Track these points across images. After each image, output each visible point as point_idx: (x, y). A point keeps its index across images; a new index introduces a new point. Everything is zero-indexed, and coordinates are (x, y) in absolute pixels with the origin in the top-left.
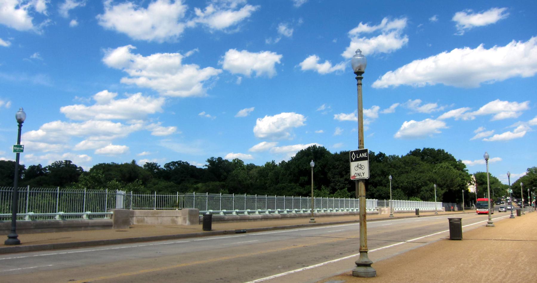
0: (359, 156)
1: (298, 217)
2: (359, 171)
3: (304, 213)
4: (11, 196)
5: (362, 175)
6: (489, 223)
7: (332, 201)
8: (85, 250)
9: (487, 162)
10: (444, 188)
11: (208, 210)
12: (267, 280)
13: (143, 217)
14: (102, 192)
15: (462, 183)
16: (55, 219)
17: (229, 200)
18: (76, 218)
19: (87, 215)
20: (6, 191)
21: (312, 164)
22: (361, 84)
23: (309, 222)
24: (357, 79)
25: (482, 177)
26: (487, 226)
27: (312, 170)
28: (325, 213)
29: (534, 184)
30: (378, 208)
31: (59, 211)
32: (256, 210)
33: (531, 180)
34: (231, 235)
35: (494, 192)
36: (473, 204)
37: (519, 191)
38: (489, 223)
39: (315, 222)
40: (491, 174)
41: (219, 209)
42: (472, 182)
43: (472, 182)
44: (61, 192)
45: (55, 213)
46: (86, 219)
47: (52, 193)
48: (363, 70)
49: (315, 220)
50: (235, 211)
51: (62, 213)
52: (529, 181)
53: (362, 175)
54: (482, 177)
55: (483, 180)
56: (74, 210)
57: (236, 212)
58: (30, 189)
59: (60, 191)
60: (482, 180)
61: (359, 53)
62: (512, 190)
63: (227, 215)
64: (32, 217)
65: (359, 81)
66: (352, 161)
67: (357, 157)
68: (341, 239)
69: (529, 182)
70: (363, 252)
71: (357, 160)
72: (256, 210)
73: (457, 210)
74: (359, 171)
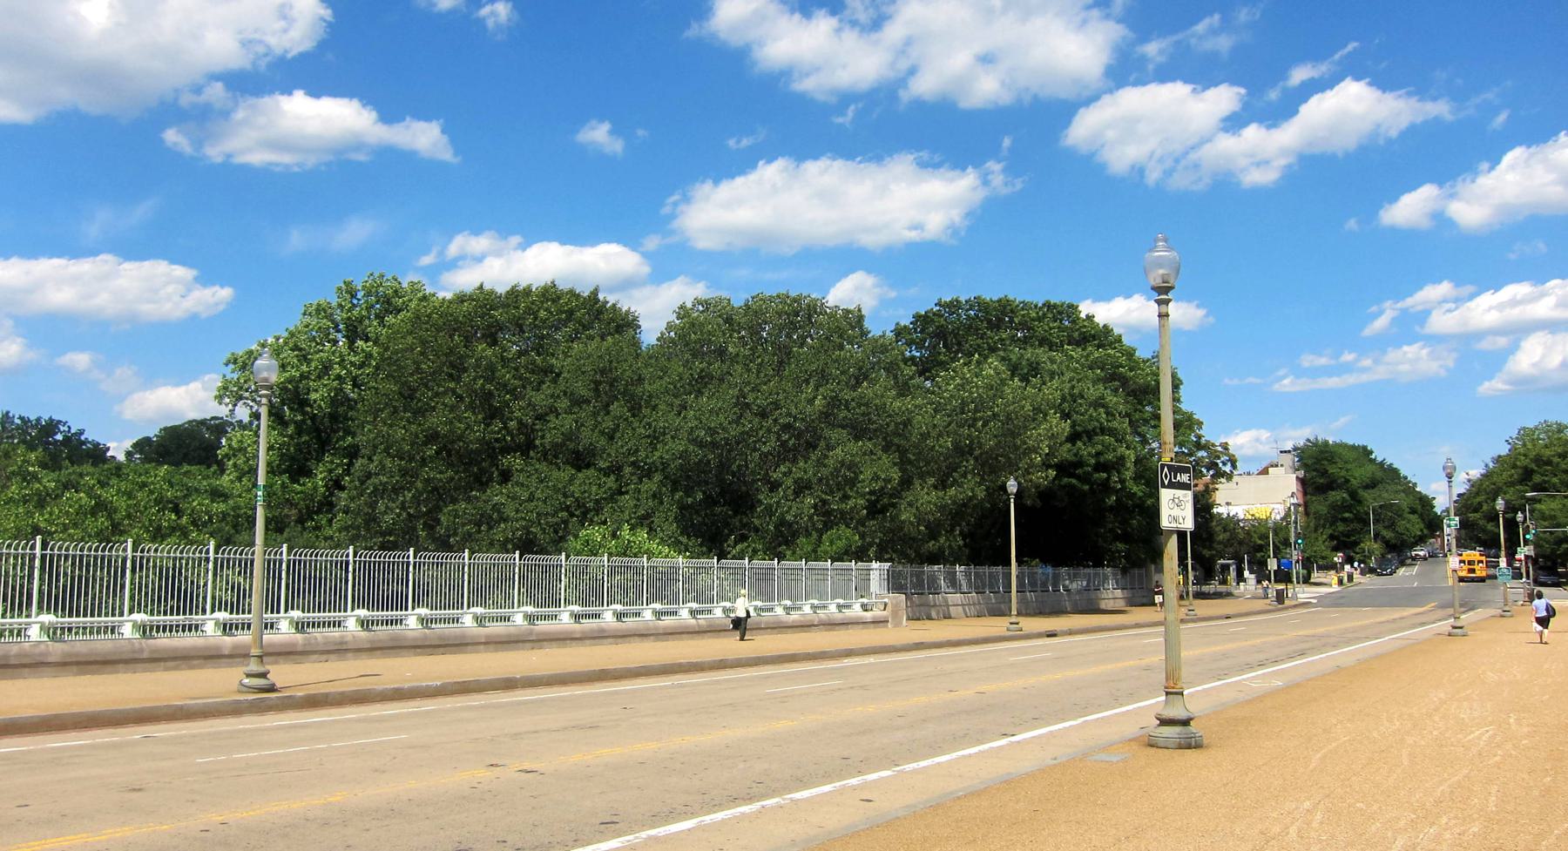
0: (1175, 478)
1: (230, 656)
2: (1176, 512)
3: (840, 611)
4: (94, 565)
5: (1181, 521)
6: (1454, 628)
7: (850, 572)
8: (610, 687)
9: (1450, 487)
10: (964, 476)
11: (469, 607)
12: (993, 748)
13: (1112, 601)
14: (482, 560)
15: (1098, 454)
16: (202, 631)
17: (552, 572)
18: (184, 631)
19: (291, 621)
20: (26, 554)
21: (1013, 485)
22: (1167, 315)
23: (235, 686)
24: (1159, 302)
25: (1326, 459)
26: (1152, 744)
27: (1012, 500)
28: (840, 616)
29: (1537, 479)
30: (886, 600)
31: (131, 611)
32: (804, 602)
33: (1523, 462)
34: (581, 688)
35: (1376, 521)
36: (1246, 574)
37: (1490, 527)
38: (1454, 628)
39: (1021, 630)
40: (1371, 452)
41: (557, 604)
42: (1224, 464)
43: (1224, 464)
44: (292, 557)
45: (121, 618)
46: (355, 629)
47: (74, 557)
48: (1172, 282)
49: (1020, 625)
50: (650, 606)
51: (140, 617)
52: (1514, 466)
53: (1181, 521)
54: (1326, 459)
55: (1331, 471)
56: (63, 609)
57: (614, 614)
58: (289, 553)
59: (46, 550)
60: (1324, 473)
61: (1161, 244)
62: (1457, 518)
63: (701, 616)
64: (49, 629)
65: (1163, 307)
66: (1164, 486)
67: (1173, 480)
68: (1382, 619)
69: (1516, 475)
70: (1173, 693)
71: (1172, 485)
72: (515, 610)
73: (1120, 604)
74: (1176, 512)
